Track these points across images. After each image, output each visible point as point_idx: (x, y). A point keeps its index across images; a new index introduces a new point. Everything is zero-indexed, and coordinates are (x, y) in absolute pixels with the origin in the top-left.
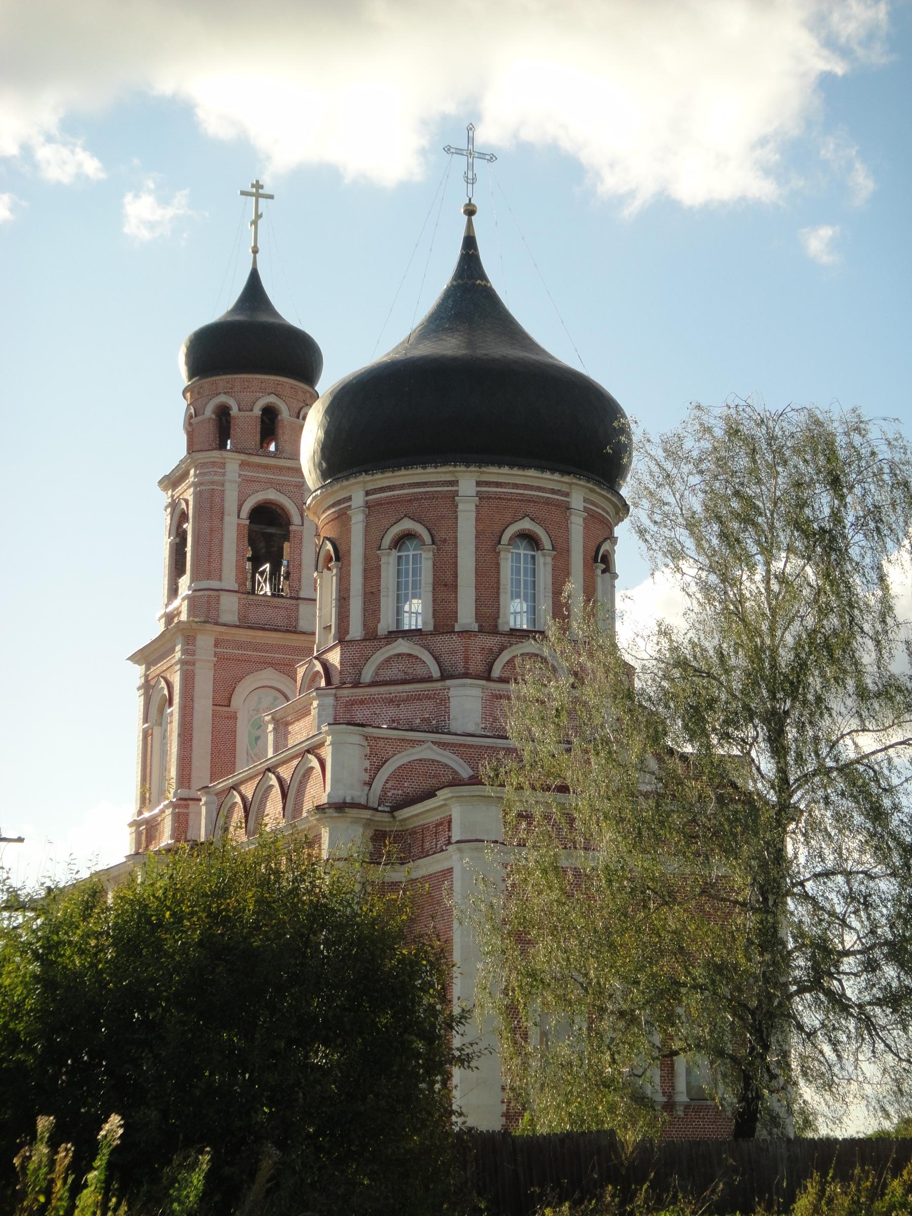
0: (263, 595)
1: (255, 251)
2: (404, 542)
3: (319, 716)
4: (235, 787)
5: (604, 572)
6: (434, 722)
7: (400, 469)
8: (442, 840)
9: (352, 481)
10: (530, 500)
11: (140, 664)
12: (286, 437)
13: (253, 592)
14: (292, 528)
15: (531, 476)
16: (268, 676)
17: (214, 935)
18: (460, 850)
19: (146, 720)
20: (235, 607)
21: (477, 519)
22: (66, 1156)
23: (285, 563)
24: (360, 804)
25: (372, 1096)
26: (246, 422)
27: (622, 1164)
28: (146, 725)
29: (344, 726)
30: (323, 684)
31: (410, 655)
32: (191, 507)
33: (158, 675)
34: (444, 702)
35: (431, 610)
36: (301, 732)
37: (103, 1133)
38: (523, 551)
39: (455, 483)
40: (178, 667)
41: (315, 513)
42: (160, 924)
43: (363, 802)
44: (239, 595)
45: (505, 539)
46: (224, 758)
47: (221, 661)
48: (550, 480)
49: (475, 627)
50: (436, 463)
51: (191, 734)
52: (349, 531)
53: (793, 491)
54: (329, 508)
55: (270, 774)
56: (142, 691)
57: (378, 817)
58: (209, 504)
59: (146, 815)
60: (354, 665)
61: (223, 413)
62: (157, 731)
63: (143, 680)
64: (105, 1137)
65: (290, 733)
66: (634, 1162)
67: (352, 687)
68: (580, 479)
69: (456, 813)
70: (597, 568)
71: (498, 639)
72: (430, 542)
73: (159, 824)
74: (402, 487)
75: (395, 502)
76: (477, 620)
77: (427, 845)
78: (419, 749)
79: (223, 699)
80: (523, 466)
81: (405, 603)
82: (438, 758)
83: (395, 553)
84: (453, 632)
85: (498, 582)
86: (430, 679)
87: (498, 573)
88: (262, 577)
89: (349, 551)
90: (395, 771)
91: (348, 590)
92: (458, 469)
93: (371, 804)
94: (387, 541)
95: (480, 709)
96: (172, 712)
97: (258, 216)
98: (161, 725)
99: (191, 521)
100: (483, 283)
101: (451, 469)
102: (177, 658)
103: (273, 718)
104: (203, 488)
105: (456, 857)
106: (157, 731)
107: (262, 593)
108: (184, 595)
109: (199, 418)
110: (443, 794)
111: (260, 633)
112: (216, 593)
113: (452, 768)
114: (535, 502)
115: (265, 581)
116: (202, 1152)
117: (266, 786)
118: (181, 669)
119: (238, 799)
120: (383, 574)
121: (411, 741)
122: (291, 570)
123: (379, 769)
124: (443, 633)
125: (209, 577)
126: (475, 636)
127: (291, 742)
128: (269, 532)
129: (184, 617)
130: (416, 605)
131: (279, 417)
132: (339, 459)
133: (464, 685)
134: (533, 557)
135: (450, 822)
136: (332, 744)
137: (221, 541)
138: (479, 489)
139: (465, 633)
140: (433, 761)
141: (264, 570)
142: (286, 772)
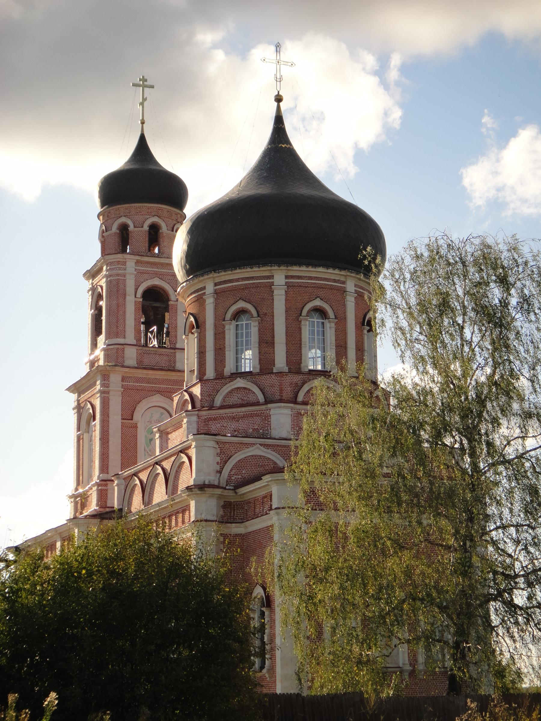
0: (153, 347)
1: (143, 123)
2: (240, 315)
3: (188, 428)
4: (136, 474)
5: (369, 331)
6: (261, 431)
7: (236, 269)
8: (267, 507)
9: (206, 277)
10: (321, 287)
11: (74, 393)
12: (165, 244)
13: (146, 345)
14: (170, 303)
15: (320, 272)
16: (157, 400)
17: (111, 584)
18: (278, 514)
19: (79, 429)
20: (135, 355)
21: (286, 300)
22: (25, 717)
23: (166, 325)
24: (214, 485)
25: (206, 677)
26: (139, 234)
27: (368, 713)
28: (79, 433)
29: (203, 436)
30: (190, 407)
31: (245, 388)
32: (104, 291)
33: (86, 400)
34: (267, 418)
35: (257, 359)
36: (177, 438)
37: (46, 703)
38: (316, 320)
39: (272, 277)
40: (99, 395)
41: (183, 297)
42: (79, 577)
43: (216, 483)
44: (137, 347)
45: (304, 312)
46: (129, 456)
47: (126, 390)
48: (332, 274)
49: (286, 369)
50: (259, 264)
51: (108, 438)
52: (204, 309)
53: (476, 287)
54: (191, 294)
55: (157, 466)
56: (76, 411)
57: (226, 493)
58: (116, 288)
59: (81, 490)
60: (209, 395)
61: (124, 229)
62: (86, 436)
63: (76, 403)
64: (48, 705)
65: (169, 439)
66: (375, 711)
67: (209, 410)
68: (352, 273)
69: (275, 490)
70: (364, 329)
71: (301, 377)
72: (256, 316)
73: (89, 496)
74: (237, 280)
75: (234, 290)
76: (287, 365)
77: (257, 510)
78: (251, 449)
79: (128, 415)
80: (315, 266)
81: (242, 354)
82: (263, 454)
83: (234, 323)
84: (272, 373)
85: (301, 340)
86: (258, 404)
87: (301, 334)
88: (152, 335)
89: (204, 322)
90: (236, 463)
91: (205, 347)
92: (273, 268)
93: (221, 485)
94: (229, 316)
95: (290, 422)
96: (95, 424)
97: (144, 99)
98: (88, 432)
99: (104, 299)
100: (288, 146)
101: (269, 268)
102: (97, 389)
103: (159, 430)
104: (111, 278)
105: (275, 518)
106: (86, 436)
107: (151, 346)
108: (101, 347)
109: (108, 233)
110: (266, 478)
111: (151, 372)
112: (122, 347)
113: (273, 461)
114: (323, 288)
115: (154, 338)
116: (105, 714)
117: (155, 474)
118: (100, 396)
119: (138, 482)
120: (227, 337)
121: (246, 444)
122: (170, 330)
123: (226, 462)
124: (266, 374)
125: (117, 336)
126: (286, 375)
127: (170, 446)
128: (155, 305)
129: (101, 363)
130: (248, 354)
131: (160, 231)
132: (197, 263)
133: (280, 407)
134: (323, 323)
135: (271, 496)
136: (196, 447)
137: (125, 312)
138: (287, 280)
139: (280, 374)
140: (260, 456)
141: (153, 331)
142: (167, 465)
